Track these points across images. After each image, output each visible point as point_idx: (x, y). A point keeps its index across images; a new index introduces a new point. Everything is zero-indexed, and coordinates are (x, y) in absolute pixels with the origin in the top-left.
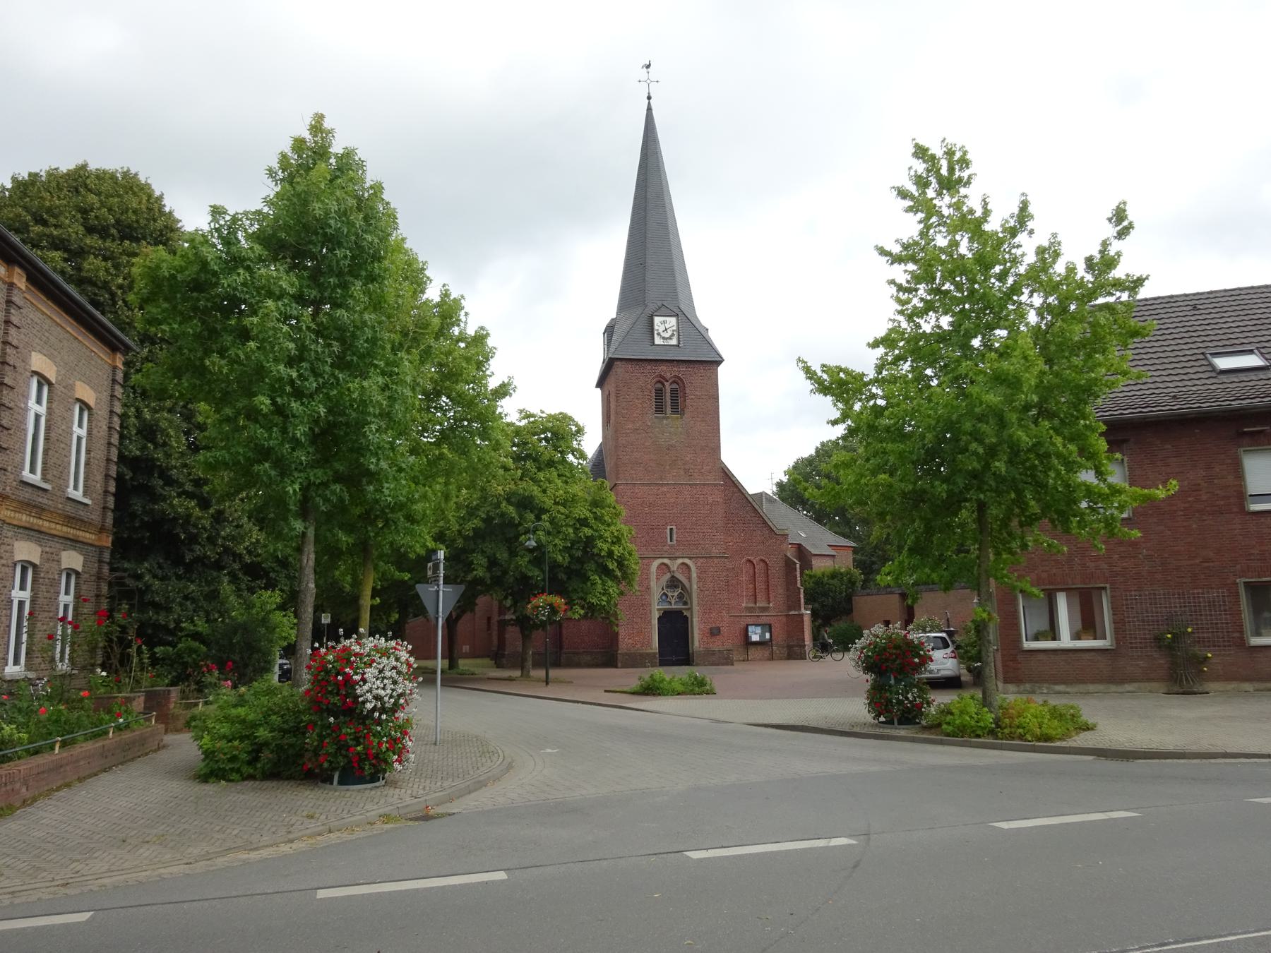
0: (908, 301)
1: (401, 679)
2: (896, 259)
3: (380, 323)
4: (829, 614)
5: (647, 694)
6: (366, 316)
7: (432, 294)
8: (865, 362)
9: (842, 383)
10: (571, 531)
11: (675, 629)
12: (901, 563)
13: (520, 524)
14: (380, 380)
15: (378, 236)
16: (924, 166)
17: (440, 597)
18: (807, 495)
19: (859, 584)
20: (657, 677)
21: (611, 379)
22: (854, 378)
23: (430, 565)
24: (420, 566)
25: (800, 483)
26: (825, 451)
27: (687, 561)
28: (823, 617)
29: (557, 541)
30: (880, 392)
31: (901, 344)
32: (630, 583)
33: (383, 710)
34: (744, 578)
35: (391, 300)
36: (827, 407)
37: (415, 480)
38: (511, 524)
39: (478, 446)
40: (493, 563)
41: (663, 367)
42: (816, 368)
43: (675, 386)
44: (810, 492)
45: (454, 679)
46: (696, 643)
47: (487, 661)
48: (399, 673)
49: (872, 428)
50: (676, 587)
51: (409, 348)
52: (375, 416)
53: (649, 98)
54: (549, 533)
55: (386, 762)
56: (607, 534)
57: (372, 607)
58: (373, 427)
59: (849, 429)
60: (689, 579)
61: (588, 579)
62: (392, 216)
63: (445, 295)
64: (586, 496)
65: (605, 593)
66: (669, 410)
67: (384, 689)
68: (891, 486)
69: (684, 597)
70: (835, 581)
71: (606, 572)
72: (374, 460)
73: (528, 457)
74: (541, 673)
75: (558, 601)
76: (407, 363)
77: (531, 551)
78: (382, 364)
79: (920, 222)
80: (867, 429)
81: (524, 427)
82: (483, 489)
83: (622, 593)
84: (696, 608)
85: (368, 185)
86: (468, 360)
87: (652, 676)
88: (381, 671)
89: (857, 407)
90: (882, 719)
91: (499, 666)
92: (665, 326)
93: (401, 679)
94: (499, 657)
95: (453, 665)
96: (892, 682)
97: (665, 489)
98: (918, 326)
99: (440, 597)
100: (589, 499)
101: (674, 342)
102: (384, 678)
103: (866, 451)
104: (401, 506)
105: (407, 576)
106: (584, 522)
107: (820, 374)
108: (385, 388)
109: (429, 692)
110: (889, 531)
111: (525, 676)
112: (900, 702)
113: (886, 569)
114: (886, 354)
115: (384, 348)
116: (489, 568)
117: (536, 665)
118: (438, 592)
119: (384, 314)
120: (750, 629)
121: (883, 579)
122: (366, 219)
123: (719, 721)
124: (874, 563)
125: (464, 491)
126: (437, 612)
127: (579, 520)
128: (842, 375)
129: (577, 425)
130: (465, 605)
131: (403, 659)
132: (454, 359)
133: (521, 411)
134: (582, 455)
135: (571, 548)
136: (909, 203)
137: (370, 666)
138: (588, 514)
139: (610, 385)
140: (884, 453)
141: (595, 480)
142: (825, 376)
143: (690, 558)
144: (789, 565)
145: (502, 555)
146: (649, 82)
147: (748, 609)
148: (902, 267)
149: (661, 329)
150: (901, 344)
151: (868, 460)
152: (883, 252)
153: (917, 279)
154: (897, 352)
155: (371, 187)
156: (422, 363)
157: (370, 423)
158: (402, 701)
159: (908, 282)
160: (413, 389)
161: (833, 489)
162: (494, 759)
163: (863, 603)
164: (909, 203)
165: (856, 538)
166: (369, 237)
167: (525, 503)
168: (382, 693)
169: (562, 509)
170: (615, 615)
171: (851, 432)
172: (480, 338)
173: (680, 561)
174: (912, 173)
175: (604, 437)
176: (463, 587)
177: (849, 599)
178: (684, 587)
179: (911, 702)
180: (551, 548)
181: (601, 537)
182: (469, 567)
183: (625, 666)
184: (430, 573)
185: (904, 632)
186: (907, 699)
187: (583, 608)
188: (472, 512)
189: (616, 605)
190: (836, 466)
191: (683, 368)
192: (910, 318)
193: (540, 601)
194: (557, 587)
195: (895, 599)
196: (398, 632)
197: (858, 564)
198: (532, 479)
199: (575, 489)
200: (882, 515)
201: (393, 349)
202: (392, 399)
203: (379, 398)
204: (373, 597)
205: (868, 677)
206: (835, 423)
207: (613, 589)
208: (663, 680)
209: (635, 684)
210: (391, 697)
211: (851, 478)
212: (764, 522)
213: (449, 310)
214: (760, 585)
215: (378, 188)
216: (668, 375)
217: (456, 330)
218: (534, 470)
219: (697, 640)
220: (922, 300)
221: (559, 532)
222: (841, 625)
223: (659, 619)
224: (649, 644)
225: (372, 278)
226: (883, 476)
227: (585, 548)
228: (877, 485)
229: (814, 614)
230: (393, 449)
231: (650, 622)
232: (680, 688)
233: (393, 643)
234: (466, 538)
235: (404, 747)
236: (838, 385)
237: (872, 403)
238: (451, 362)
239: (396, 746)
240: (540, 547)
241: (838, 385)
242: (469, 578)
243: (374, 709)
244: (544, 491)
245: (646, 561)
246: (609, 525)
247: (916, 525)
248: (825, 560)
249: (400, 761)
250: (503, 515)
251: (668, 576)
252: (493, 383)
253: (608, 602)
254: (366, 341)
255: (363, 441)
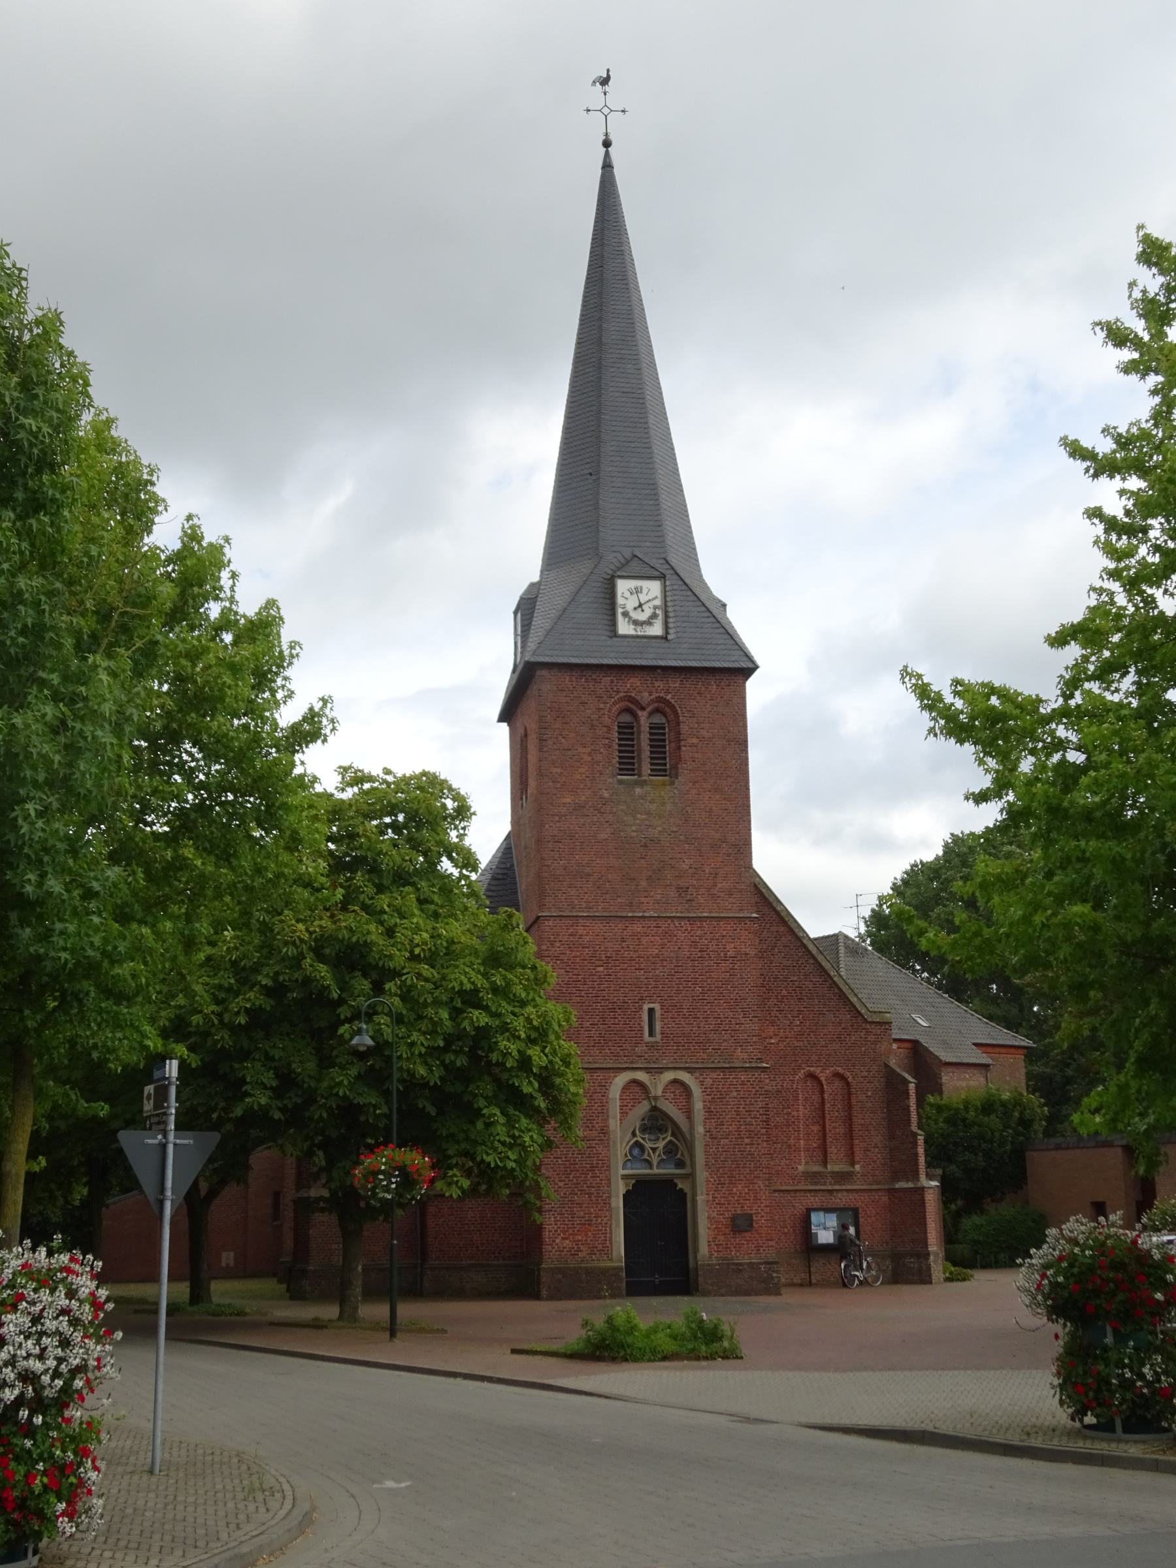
0: (1130, 553)
1: (78, 1336)
2: (1103, 467)
3: (51, 594)
4: (981, 1187)
5: (599, 1359)
6: (22, 582)
7: (164, 535)
8: (1040, 677)
9: (994, 718)
10: (445, 1015)
11: (659, 1212)
12: (1123, 1088)
13: (341, 1002)
14: (49, 710)
15: (50, 421)
16: (1161, 279)
17: (168, 1156)
18: (923, 944)
19: (1039, 1126)
20: (620, 1320)
21: (530, 705)
22: (1019, 706)
23: (149, 1089)
24: (129, 1087)
25: (910, 920)
26: (959, 851)
27: (684, 1076)
28: (962, 1195)
29: (415, 1036)
30: (1073, 737)
31: (1116, 638)
32: (566, 1124)
33: (39, 1404)
34: (802, 1111)
35: (76, 547)
36: (966, 766)
37: (123, 917)
38: (317, 998)
39: (256, 841)
40: (287, 1080)
41: (634, 683)
42: (941, 685)
43: (658, 719)
44: (933, 938)
45: (198, 1325)
46: (704, 1249)
47: (269, 1285)
48: (75, 1322)
49: (1055, 811)
50: (661, 1130)
51: (111, 645)
52: (36, 784)
53: (607, 144)
54: (399, 1020)
55: (41, 1515)
56: (519, 1024)
57: (31, 1177)
58: (31, 807)
59: (1010, 810)
60: (689, 1113)
61: (478, 1113)
62: (80, 378)
63: (192, 536)
64: (475, 942)
65: (516, 1143)
66: (646, 768)
67: (41, 1357)
68: (1095, 928)
69: (679, 1150)
70: (994, 1121)
71: (520, 1101)
72: (31, 876)
73: (358, 862)
74: (378, 1311)
75: (417, 1160)
76: (104, 677)
77: (361, 1055)
78: (55, 678)
79: (1154, 392)
80: (1044, 816)
81: (350, 804)
82: (265, 928)
83: (548, 1145)
84: (702, 1175)
85: (30, 317)
86: (235, 669)
87: (610, 1320)
88: (36, 1320)
89: (1026, 765)
90: (1089, 1419)
91: (296, 1295)
92: (638, 598)
93: (78, 1336)
94: (297, 1280)
95: (198, 1294)
96: (1109, 1340)
97: (638, 928)
98: (1150, 602)
99: (168, 1156)
100: (482, 948)
101: (657, 630)
102: (42, 1334)
103: (1046, 857)
104: (90, 969)
105: (103, 1110)
106: (472, 999)
107: (949, 698)
108: (58, 728)
109: (140, 1354)
110: (1096, 1021)
111: (348, 1317)
112: (1126, 1385)
113: (1090, 1101)
114: (1085, 659)
115: (59, 646)
116: (278, 1093)
117: (371, 1294)
118: (163, 1147)
119: (59, 576)
120: (815, 1218)
121: (1087, 1118)
122: (26, 385)
123: (748, 1420)
124: (1068, 1081)
125: (228, 934)
126: (162, 1189)
127: (461, 993)
128: (994, 701)
129: (458, 797)
130: (225, 1167)
131: (84, 1292)
132: (207, 667)
133: (344, 770)
134: (467, 860)
135: (445, 1049)
136: (1129, 354)
137: (14, 1308)
138: (480, 982)
139: (528, 716)
140: (1083, 859)
141: (494, 911)
142: (959, 704)
143: (690, 1070)
144: (893, 1085)
145: (304, 1066)
146: (606, 112)
147: (811, 1176)
148: (1117, 483)
149: (631, 603)
150: (1116, 638)
151: (1049, 875)
152: (1076, 451)
153: (1145, 506)
154: (1107, 654)
155: (38, 322)
156: (139, 673)
157: (24, 801)
158: (78, 1383)
159: (1128, 513)
160: (118, 730)
161: (977, 934)
162: (274, 1504)
163: (1048, 1166)
164: (1129, 354)
165: (1036, 1028)
166: (29, 421)
167: (351, 958)
168: (36, 1366)
169: (425, 970)
170: (537, 1188)
171: (1015, 817)
172: (263, 628)
173: (669, 1076)
174: (1137, 294)
175: (515, 821)
176: (215, 1137)
177: (1019, 1156)
178: (677, 1131)
179: (1149, 1384)
180: (403, 1051)
181: (504, 1028)
182: (236, 1088)
183: (554, 1296)
184: (148, 1106)
185: (1132, 1234)
186: (1142, 1376)
187: (468, 1173)
188: (244, 974)
189: (537, 1169)
190: (984, 886)
191: (675, 683)
192: (1132, 585)
193: (382, 1160)
194: (414, 1129)
195: (1115, 1156)
196: (82, 1237)
197: (1037, 1083)
198: (365, 908)
199: (455, 929)
200: (1080, 989)
201: (78, 647)
202: (72, 751)
203: (46, 748)
204: (32, 1155)
205: (1057, 1328)
206: (981, 798)
207: (531, 1137)
208: (634, 1328)
209: (574, 1335)
210: (56, 1374)
211: (1016, 912)
212: (842, 996)
213: (199, 567)
214: (836, 1128)
215: (50, 325)
216: (645, 698)
217: (214, 610)
218: (370, 890)
219: (706, 1239)
220: (1157, 548)
221: (420, 1017)
222: (1003, 1210)
223: (626, 1196)
224: (606, 1249)
225: (36, 504)
226: (1078, 908)
227: (473, 1049)
228: (1067, 925)
229: (948, 1190)
230: (74, 852)
231: (607, 1203)
232: (670, 1346)
233: (64, 1258)
234: (235, 1029)
235: (81, 1482)
236: (985, 721)
237: (1056, 757)
238: (210, 672)
239: (67, 1485)
240: (381, 1047)
241: (985, 721)
242: (238, 1112)
243: (19, 1401)
244: (390, 933)
245: (599, 1076)
246: (523, 1004)
247: (1153, 1008)
248: (967, 1074)
249: (70, 1514)
250: (307, 981)
251: (644, 1108)
252: (288, 715)
253: (520, 1162)
254: (23, 632)
255: (11, 837)
